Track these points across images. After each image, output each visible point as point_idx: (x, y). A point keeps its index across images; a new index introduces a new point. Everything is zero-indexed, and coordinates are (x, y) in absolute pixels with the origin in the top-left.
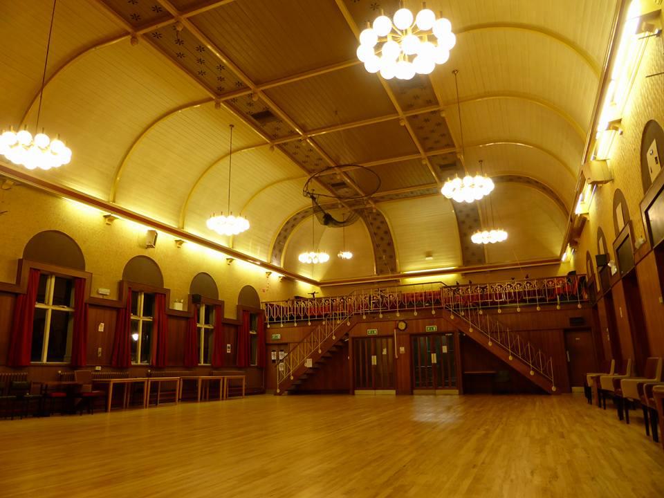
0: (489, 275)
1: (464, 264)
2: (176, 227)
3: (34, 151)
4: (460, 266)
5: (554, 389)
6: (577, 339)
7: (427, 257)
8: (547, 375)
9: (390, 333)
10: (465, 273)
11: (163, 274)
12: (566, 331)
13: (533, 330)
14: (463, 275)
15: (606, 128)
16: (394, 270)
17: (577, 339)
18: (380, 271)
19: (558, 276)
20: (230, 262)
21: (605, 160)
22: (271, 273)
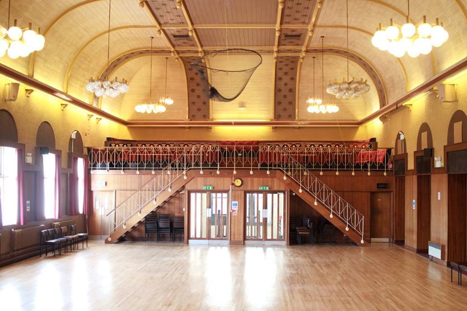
0: (297, 130)
1: (275, 118)
2: (27, 75)
3: (15, 44)
4: (271, 120)
5: (362, 242)
6: (379, 200)
7: (240, 107)
8: (359, 231)
9: (226, 189)
10: (276, 127)
11: (18, 127)
12: (373, 193)
13: (348, 192)
14: (273, 128)
15: (434, 45)
16: (206, 116)
17: (379, 200)
18: (192, 117)
19: (355, 139)
20: (64, 108)
21: (454, 85)
22: (92, 115)
